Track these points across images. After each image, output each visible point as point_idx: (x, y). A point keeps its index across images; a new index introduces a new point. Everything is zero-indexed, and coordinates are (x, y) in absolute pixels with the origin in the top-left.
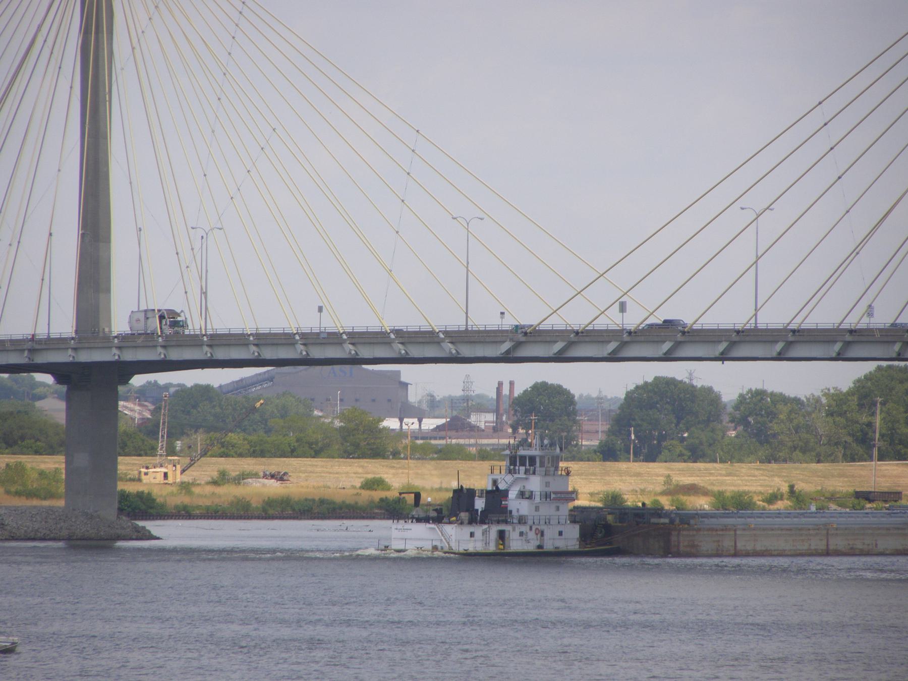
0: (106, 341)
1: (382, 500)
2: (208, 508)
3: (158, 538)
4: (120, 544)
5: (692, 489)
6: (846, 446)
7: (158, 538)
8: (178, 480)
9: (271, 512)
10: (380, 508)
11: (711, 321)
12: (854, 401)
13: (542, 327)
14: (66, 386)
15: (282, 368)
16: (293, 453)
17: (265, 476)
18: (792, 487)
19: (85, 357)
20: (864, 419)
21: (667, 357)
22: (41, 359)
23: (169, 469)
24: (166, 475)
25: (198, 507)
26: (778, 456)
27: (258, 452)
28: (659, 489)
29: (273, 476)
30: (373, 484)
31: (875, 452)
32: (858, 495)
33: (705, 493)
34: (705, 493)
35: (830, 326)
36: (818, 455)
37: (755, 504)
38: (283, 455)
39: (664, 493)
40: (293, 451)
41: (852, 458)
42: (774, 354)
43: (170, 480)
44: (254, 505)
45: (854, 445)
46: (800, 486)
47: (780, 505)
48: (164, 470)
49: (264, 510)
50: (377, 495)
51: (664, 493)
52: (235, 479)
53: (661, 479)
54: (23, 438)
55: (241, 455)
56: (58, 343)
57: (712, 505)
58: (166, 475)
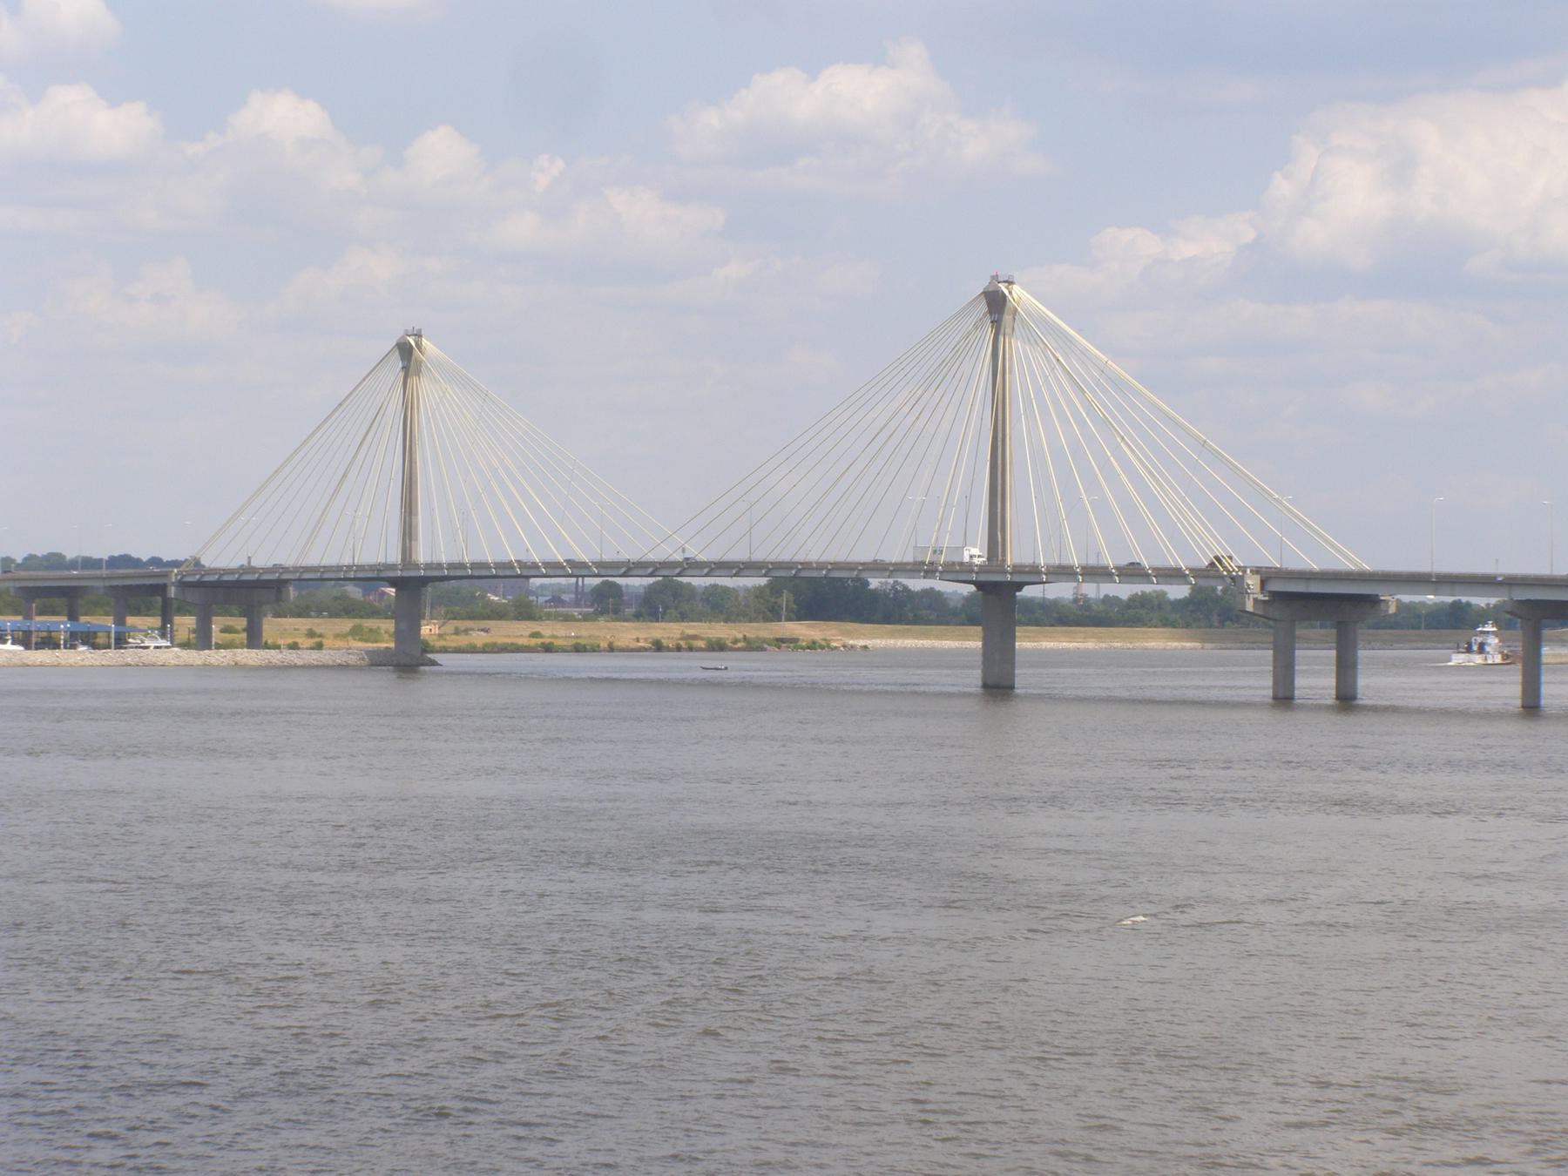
0: (417, 567)
1: (542, 643)
2: (455, 648)
3: (441, 665)
4: (422, 668)
5: (695, 637)
6: (764, 613)
7: (441, 665)
8: (437, 632)
9: (487, 649)
10: (540, 647)
11: (702, 557)
12: (768, 591)
13: (642, 560)
14: (980, 628)
15: (1539, 598)
16: (489, 618)
17: (478, 630)
18: (745, 636)
19: (406, 574)
20: (773, 600)
21: (707, 575)
22: (383, 575)
23: (432, 627)
24: (431, 630)
25: (450, 647)
26: (596, 605)
27: (472, 617)
28: (679, 636)
29: (482, 630)
30: (535, 635)
31: (783, 618)
32: (778, 640)
33: (702, 639)
34: (702, 639)
35: (761, 560)
36: (750, 618)
37: (726, 645)
38: (484, 619)
39: (681, 639)
40: (489, 616)
41: (766, 620)
42: (703, 574)
43: (433, 632)
44: (478, 646)
45: (768, 613)
46: (748, 635)
47: (739, 645)
48: (429, 627)
49: (483, 648)
50: (539, 641)
51: (681, 639)
52: (463, 631)
53: (679, 632)
54: (353, 610)
55: (462, 619)
56: (393, 567)
57: (705, 645)
58: (431, 630)
